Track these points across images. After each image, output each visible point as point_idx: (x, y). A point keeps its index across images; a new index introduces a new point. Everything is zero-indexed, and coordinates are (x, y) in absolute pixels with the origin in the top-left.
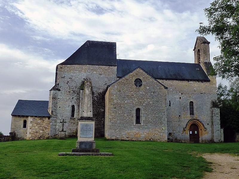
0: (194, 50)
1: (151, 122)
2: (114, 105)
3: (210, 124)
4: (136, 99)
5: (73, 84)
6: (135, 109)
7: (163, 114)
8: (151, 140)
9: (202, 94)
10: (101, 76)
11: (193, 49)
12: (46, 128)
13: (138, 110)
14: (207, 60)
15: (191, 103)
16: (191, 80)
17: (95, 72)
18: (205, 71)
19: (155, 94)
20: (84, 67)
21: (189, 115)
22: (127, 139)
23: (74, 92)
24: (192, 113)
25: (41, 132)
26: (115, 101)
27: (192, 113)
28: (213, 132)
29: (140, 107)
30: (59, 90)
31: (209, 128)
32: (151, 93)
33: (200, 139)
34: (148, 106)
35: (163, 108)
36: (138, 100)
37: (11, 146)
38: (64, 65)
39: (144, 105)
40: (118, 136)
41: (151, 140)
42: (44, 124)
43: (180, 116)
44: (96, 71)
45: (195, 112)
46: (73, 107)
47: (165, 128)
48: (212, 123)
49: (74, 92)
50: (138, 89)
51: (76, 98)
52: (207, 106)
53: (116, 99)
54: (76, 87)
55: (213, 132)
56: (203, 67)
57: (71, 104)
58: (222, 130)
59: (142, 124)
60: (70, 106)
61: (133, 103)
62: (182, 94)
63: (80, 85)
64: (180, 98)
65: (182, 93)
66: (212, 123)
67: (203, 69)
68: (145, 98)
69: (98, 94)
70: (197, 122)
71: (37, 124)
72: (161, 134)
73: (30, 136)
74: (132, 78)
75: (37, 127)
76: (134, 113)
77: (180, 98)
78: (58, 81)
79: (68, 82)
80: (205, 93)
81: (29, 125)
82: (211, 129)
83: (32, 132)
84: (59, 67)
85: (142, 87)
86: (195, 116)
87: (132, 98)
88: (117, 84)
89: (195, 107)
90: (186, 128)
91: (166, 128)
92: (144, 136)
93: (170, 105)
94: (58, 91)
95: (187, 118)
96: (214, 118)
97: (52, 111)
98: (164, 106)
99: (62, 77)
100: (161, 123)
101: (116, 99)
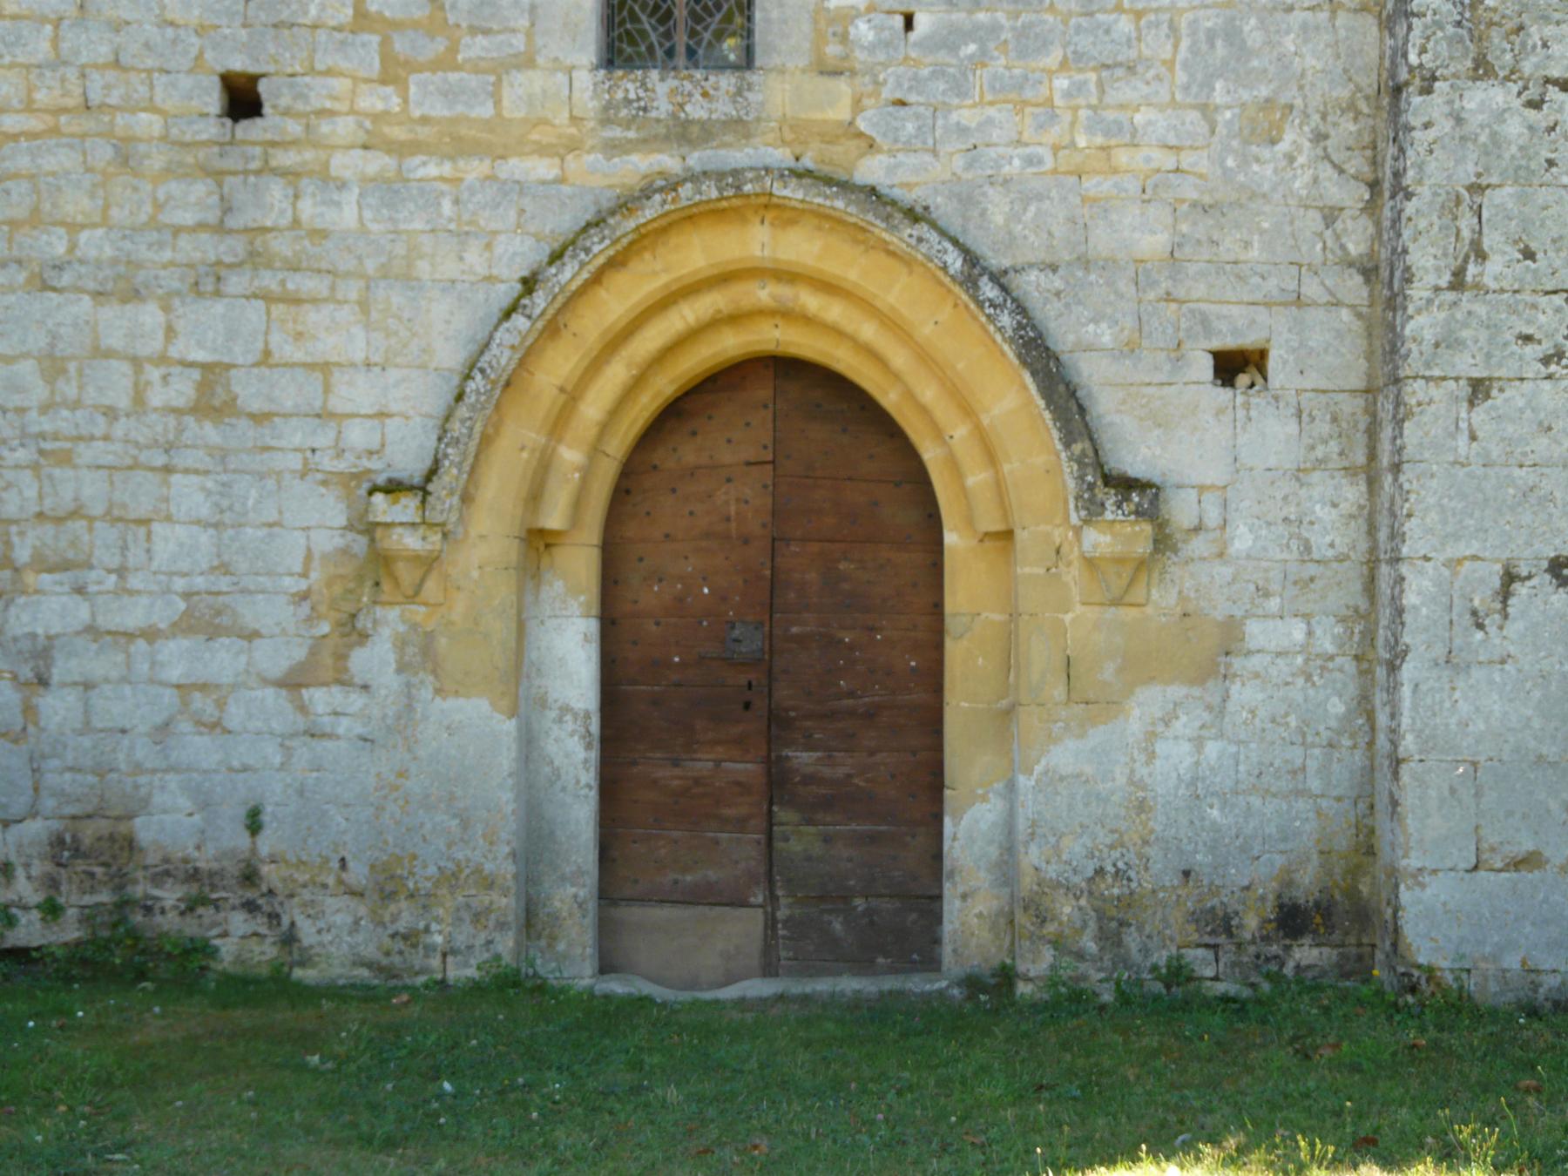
3: (1315, 352)
33: (970, 829)
43: (242, 100)
70: (828, 287)
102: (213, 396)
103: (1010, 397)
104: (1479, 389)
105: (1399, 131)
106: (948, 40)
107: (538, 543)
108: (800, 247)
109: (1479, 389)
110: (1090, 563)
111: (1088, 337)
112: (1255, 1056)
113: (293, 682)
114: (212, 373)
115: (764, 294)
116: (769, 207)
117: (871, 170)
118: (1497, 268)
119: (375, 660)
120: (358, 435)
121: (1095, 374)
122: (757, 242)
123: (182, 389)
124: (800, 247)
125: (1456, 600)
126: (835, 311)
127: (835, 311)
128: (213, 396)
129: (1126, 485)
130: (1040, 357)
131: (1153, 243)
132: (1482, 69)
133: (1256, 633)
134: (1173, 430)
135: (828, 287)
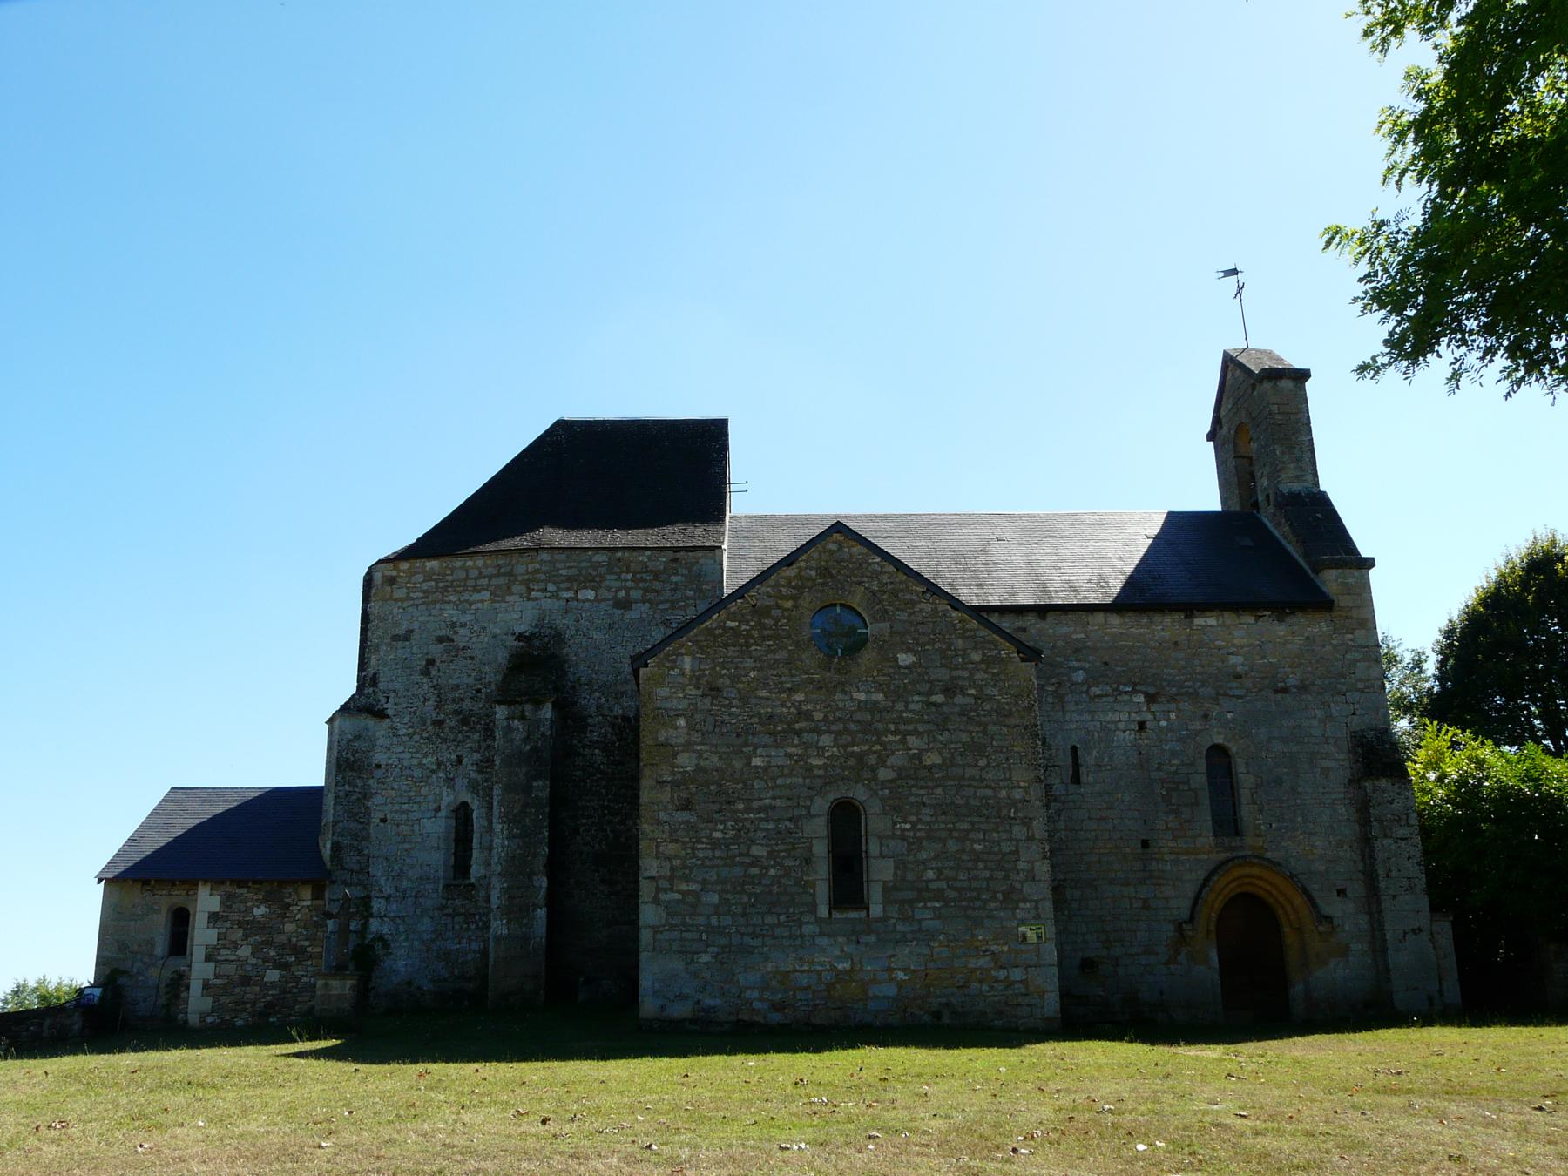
0: (1211, 436)
1: (939, 895)
2: (676, 785)
3: (1357, 888)
4: (826, 740)
5: (460, 675)
6: (821, 805)
7: (1018, 831)
8: (946, 1020)
9: (1285, 690)
10: (633, 615)
11: (1208, 429)
12: (299, 951)
13: (845, 818)
14: (1298, 478)
15: (1219, 757)
16: (1205, 608)
17: (590, 594)
18: (1290, 548)
19: (959, 699)
20: (520, 569)
21: (1207, 839)
22: (776, 1017)
23: (465, 721)
24: (1228, 823)
25: (272, 976)
26: (686, 761)
27: (1228, 823)
28: (1379, 947)
29: (859, 793)
30: (381, 715)
31: (1346, 913)
32: (930, 693)
33: (1297, 990)
34: (912, 782)
35: (1018, 795)
36: (845, 747)
37: (1232, 859)
38: (405, 566)
39: (884, 774)
40: (708, 1001)
41: (946, 1020)
42: (289, 927)
43: (1145, 844)
44: (595, 589)
45: (1246, 811)
46: (462, 814)
47: (1036, 931)
48: (1371, 879)
49: (465, 721)
50: (838, 671)
51: (477, 756)
52: (1326, 771)
53: (688, 745)
54: (479, 691)
55: (1379, 947)
56: (1278, 525)
57: (448, 799)
58: (1445, 928)
59: (876, 910)
60: (443, 813)
61: (809, 769)
62: (1151, 699)
63: (499, 678)
64: (1142, 726)
65: (1152, 690)
66: (1371, 879)
67: (1280, 538)
68: (892, 727)
69: (613, 725)
70: (1260, 878)
71: (250, 927)
72: (1017, 974)
73: (207, 1003)
74: (795, 598)
75: (245, 951)
76: (817, 832)
77: (1142, 726)
78: (373, 662)
79: (431, 662)
80: (1303, 688)
81: (202, 935)
82: (1363, 921)
83: (218, 982)
84: (378, 577)
85: (868, 656)
86: (1249, 840)
87: (799, 733)
88: (695, 643)
89: (1246, 780)
90: (1192, 919)
91: (1049, 930)
92: (890, 990)
93: (1076, 779)
94: (370, 722)
95: (1189, 855)
96: (1384, 846)
97: (337, 847)
98: (1022, 775)
99: (396, 638)
100: (1011, 898)
101: (688, 745)
102: (1146, 905)
103: (1299, 900)
104: (1394, 897)
105: (1372, 849)
106: (1279, 829)
107: (1208, 932)
108: (1256, 871)
109: (1394, 897)
110: (1320, 934)
111: (1314, 887)
112: (426, 925)
113: (1167, 964)
114: (1145, 901)
115: (1247, 880)
116: (1252, 865)
117: (1268, 855)
118: (1394, 873)
119: (1182, 958)
120: (1175, 912)
121: (1315, 894)
122: (1247, 870)
123: (1140, 904)
124: (1256, 871)
125: (1244, 1121)
126: (1261, 883)
127: (1261, 883)
128: (1146, 905)
129: (1326, 917)
130: (1305, 892)
131: (1323, 868)
132: (1386, 836)
133: (1353, 946)
134: (1334, 907)
135: (1260, 878)
